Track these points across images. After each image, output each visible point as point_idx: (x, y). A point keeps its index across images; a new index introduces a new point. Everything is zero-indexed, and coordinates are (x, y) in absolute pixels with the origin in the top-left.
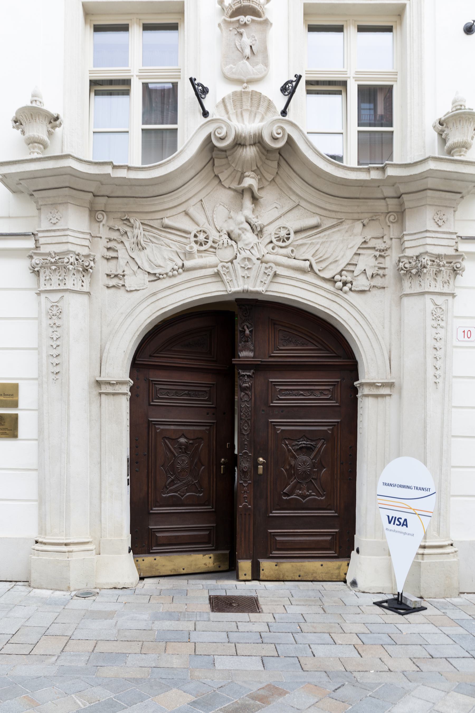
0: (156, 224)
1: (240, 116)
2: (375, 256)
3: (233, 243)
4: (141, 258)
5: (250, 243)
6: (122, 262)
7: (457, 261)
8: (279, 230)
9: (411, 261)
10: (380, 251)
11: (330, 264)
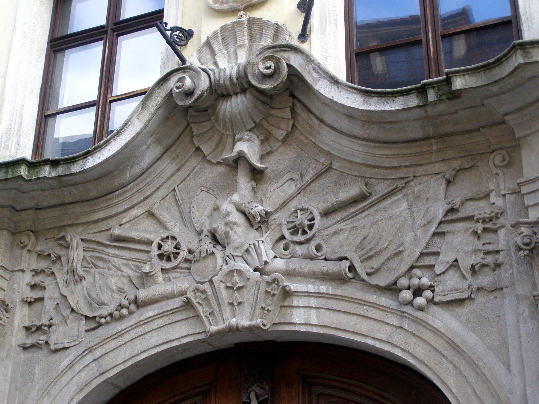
0: (103, 238)
1: (233, 55)
2: (475, 233)
5: (242, 245)
6: (49, 305)
8: (296, 215)
10: (484, 221)
11: (388, 259)
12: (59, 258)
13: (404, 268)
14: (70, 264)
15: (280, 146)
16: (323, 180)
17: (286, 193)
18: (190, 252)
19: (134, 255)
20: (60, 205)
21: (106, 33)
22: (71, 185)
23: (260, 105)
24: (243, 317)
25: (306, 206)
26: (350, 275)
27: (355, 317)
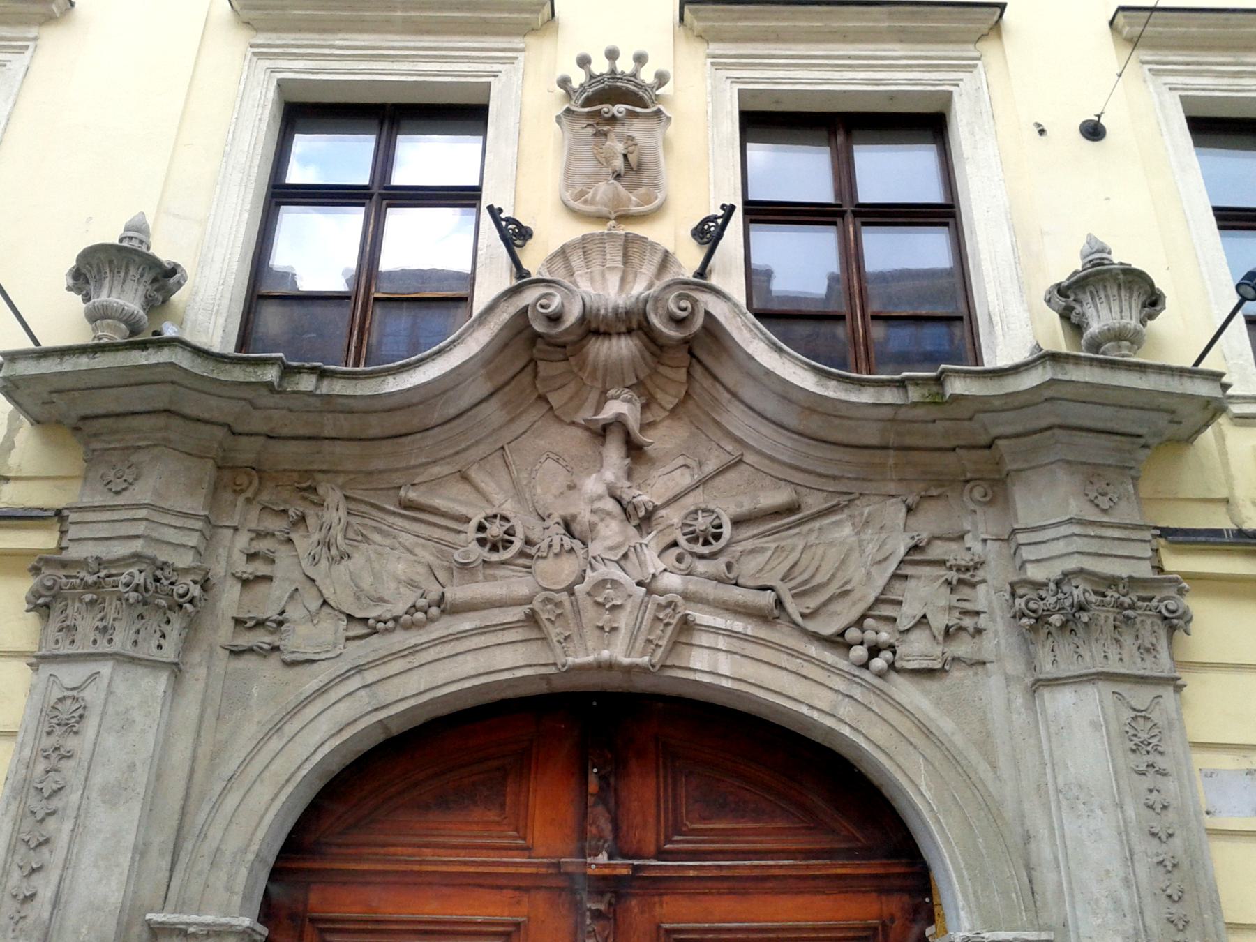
3: (577, 544)
4: (337, 583)
7: (1166, 593)
9: (1043, 593)
10: (958, 570)
12: (303, 518)
14: (324, 530)
17: (677, 484)
18: (528, 542)
19: (437, 533)
21: (370, 197)
22: (342, 412)
23: (647, 354)
24: (613, 647)
25: (711, 507)
26: (776, 612)
27: (784, 672)
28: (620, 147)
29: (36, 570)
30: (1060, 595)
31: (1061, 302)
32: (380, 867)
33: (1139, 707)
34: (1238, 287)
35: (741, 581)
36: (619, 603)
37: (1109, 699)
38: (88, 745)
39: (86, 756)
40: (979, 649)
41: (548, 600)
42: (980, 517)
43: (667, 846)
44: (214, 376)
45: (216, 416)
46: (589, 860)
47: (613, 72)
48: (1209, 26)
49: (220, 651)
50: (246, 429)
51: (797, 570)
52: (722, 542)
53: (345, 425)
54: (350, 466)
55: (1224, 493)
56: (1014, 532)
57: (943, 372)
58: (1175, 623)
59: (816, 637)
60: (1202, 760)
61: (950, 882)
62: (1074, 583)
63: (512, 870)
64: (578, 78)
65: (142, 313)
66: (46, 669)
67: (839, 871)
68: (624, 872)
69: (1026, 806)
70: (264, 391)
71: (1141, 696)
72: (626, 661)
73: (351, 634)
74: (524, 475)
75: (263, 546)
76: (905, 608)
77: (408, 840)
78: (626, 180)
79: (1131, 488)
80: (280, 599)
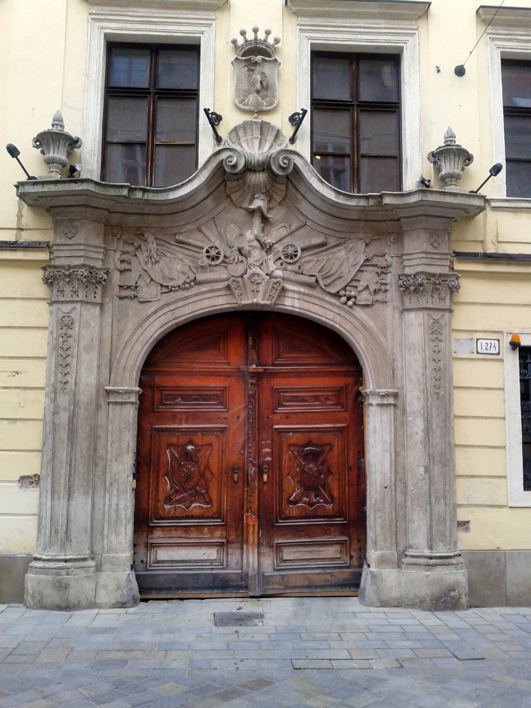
2: (377, 273)
3: (244, 259)
4: (155, 272)
9: (409, 278)
10: (382, 268)
12: (140, 246)
13: (343, 285)
14: (149, 252)
15: (277, 206)
16: (302, 230)
18: (225, 257)
19: (191, 253)
20: (139, 214)
23: (270, 180)
24: (259, 298)
25: (294, 244)
26: (316, 285)
27: (317, 306)
28: (259, 78)
29: (44, 268)
30: (415, 280)
31: (432, 159)
32: (178, 370)
33: (436, 319)
34: (490, 171)
35: (304, 273)
36: (259, 281)
37: (426, 316)
38: (77, 333)
39: (77, 337)
40: (386, 297)
41: (234, 281)
42: (392, 247)
43: (276, 362)
44: (104, 193)
45: (102, 206)
46: (249, 367)
47: (256, 39)
48: (519, 16)
49: (116, 297)
50: (115, 210)
51: (324, 268)
52: (298, 258)
53: (153, 210)
54: (155, 225)
55: (482, 239)
56: (403, 255)
57: (382, 194)
58: (453, 290)
59: (329, 294)
60: (455, 335)
61: (367, 373)
62: (420, 276)
63: (223, 370)
64: (241, 41)
65: (67, 160)
66: (56, 306)
67: (332, 370)
68: (262, 370)
69: (395, 350)
70: (123, 198)
71: (437, 315)
72: (262, 303)
73: (162, 291)
74: (222, 229)
75: (126, 257)
76: (361, 283)
77: (187, 361)
78: (261, 93)
79: (447, 238)
80: (135, 278)
